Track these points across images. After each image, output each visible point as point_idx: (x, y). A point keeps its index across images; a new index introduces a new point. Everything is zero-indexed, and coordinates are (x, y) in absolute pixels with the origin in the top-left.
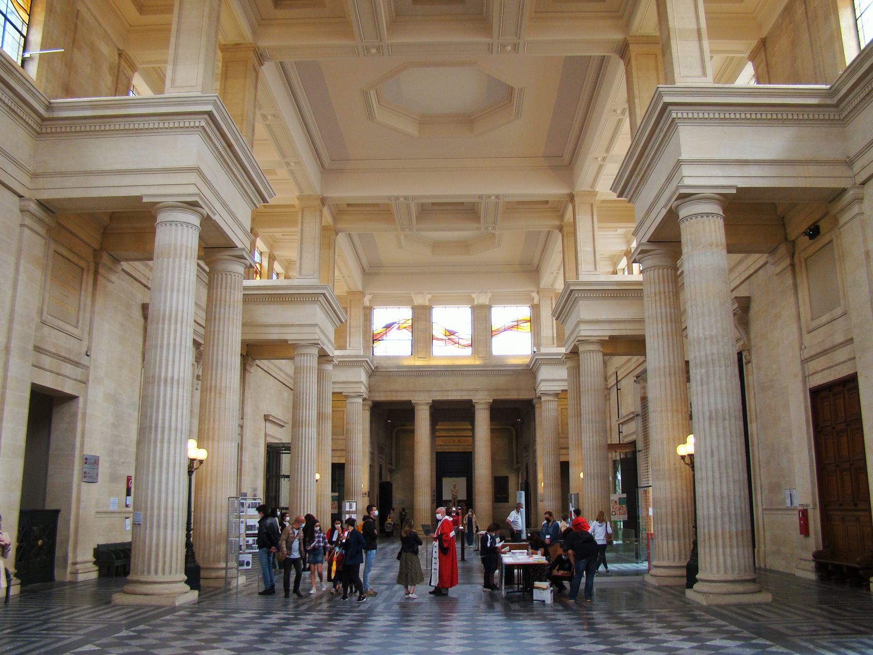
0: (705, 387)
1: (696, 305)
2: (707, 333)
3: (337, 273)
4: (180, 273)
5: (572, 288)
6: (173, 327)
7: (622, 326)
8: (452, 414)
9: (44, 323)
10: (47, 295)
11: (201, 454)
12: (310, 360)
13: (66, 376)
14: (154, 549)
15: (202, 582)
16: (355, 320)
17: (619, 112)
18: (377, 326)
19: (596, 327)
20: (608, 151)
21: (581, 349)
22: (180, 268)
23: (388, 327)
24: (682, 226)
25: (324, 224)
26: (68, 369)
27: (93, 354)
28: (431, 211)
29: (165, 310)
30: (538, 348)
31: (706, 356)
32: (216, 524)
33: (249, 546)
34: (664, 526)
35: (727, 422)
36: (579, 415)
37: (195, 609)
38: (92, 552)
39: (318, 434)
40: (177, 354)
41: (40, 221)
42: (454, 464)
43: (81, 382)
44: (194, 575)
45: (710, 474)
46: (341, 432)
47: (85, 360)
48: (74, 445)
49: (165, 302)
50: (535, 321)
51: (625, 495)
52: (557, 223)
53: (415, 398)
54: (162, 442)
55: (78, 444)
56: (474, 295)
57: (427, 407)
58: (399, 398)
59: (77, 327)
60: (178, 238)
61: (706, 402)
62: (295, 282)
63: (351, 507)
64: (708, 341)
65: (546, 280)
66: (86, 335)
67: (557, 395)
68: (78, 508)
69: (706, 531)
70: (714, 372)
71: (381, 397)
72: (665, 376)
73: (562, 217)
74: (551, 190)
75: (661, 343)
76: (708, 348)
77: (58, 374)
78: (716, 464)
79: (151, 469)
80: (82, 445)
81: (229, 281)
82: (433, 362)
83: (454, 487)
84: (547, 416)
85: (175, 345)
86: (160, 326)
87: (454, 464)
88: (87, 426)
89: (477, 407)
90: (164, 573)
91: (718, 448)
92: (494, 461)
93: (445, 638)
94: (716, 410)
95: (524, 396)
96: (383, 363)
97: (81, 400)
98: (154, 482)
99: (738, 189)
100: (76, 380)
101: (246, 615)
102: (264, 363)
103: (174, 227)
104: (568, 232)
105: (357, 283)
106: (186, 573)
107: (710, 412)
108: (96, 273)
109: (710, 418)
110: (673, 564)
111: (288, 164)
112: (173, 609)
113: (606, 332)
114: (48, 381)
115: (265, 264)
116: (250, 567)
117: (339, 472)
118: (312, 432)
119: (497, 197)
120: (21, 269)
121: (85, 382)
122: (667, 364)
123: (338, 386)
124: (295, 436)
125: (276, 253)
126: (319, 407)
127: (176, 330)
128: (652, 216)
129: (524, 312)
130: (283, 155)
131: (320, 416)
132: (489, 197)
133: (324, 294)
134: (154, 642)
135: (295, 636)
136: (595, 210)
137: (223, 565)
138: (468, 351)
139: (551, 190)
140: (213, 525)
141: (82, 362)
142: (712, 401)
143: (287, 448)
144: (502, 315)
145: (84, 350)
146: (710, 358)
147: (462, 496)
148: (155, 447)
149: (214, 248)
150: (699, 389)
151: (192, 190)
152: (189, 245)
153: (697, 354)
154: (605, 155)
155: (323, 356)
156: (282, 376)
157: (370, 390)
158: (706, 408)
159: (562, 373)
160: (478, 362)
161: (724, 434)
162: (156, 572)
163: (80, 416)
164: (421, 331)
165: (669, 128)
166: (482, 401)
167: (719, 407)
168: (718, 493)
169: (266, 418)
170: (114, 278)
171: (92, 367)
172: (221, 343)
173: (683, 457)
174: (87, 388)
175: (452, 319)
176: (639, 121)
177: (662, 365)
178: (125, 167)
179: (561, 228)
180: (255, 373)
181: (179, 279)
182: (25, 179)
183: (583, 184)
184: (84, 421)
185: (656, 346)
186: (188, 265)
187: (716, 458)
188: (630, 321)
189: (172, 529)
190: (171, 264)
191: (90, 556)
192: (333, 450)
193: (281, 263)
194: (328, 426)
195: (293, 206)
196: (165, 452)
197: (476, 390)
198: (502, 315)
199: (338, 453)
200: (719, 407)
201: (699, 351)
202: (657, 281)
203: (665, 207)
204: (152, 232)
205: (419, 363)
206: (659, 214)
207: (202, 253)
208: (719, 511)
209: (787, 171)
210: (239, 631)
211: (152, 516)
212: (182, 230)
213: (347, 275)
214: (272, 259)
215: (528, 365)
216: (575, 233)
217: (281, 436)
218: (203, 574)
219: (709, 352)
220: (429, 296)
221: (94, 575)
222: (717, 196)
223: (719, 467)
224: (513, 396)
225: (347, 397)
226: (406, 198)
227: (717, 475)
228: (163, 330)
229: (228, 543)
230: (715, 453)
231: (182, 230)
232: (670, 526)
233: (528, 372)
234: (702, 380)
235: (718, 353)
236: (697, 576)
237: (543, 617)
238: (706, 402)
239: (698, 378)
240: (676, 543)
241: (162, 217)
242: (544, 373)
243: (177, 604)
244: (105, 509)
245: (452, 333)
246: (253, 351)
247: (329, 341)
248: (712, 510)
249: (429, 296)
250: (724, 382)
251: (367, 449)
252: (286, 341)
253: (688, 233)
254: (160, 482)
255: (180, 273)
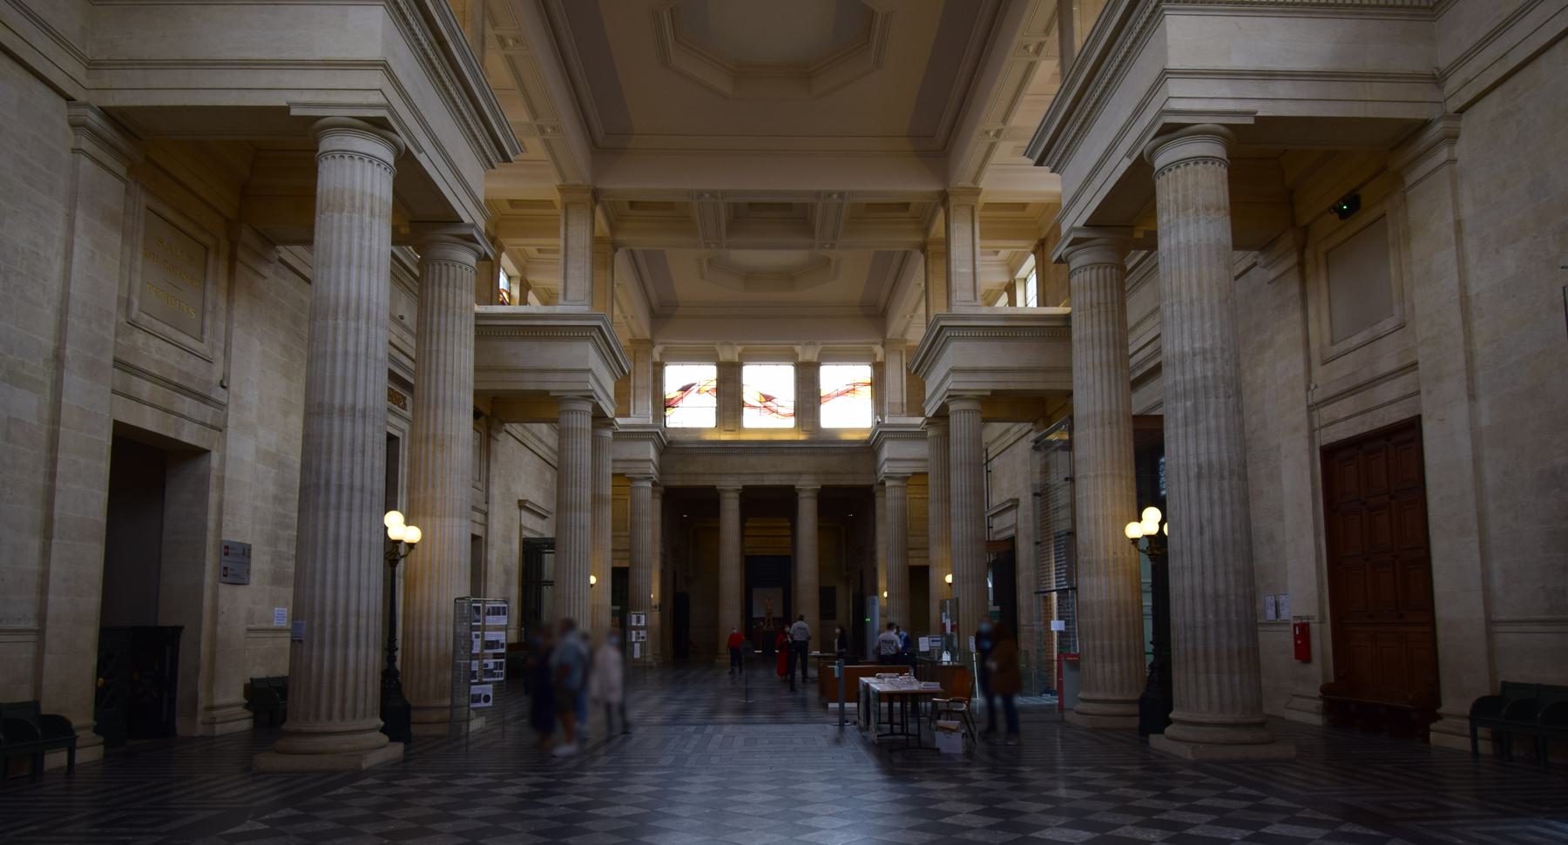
0: (1190, 429)
1: (1180, 303)
2: (1197, 345)
3: (616, 311)
4: (362, 237)
5: (942, 323)
6: (352, 325)
7: (1009, 377)
8: (772, 504)
9: (133, 324)
10: (138, 281)
11: (412, 534)
12: (582, 421)
13: (183, 416)
14: (326, 679)
15: (414, 729)
16: (643, 379)
17: (1031, 49)
18: (671, 389)
19: (973, 378)
20: (1005, 120)
21: (952, 408)
22: (362, 230)
23: (685, 389)
24: (1160, 182)
25: (598, 234)
26: (187, 405)
27: (234, 385)
28: (750, 216)
29: (337, 298)
30: (883, 418)
31: (1195, 380)
32: (437, 641)
33: (489, 673)
34: (1098, 643)
35: (1226, 483)
36: (946, 499)
37: (390, 773)
38: (241, 690)
39: (594, 524)
40: (362, 369)
41: (113, 149)
42: (771, 571)
43: (212, 427)
44: (397, 715)
45: (1197, 561)
46: (625, 528)
47: (218, 394)
48: (205, 527)
49: (338, 284)
50: (878, 384)
51: (997, 608)
52: (919, 239)
53: (723, 483)
54: (338, 508)
55: (211, 524)
56: (798, 349)
57: (736, 495)
58: (700, 483)
59: (202, 341)
60: (358, 183)
61: (1192, 451)
62: (558, 309)
63: (638, 620)
64: (1199, 358)
65: (895, 327)
66: (219, 355)
67: (905, 478)
68: (215, 622)
69: (1190, 645)
70: (1207, 405)
71: (677, 481)
72: (1103, 425)
73: (926, 230)
74: (914, 185)
75: (1098, 377)
76: (1198, 369)
77: (167, 411)
78: (1207, 547)
79: (319, 553)
80: (219, 525)
81: (452, 275)
82: (744, 437)
83: (767, 604)
84: (889, 506)
85: (356, 355)
86: (331, 322)
87: (771, 571)
88: (226, 496)
89: (801, 495)
90: (343, 717)
91: (1211, 521)
92: (822, 570)
93: (811, 816)
94: (1210, 463)
95: (862, 481)
96: (678, 437)
97: (215, 458)
98: (324, 573)
99: (1258, 119)
100: (203, 424)
101: (477, 781)
102: (516, 428)
103: (347, 160)
104: (937, 253)
105: (643, 328)
106: (382, 718)
107: (1200, 467)
108: (232, 259)
109: (1199, 476)
110: (1112, 697)
111: (542, 130)
112: (359, 774)
113: (986, 384)
114: (149, 421)
115: (516, 292)
116: (490, 704)
117: (621, 579)
118: (586, 518)
119: (841, 195)
120: (79, 224)
121: (220, 429)
122: (1107, 408)
123: (620, 465)
124: (559, 526)
125: (531, 279)
126: (594, 487)
127: (357, 330)
128: (1097, 182)
129: (864, 372)
130: (534, 113)
131: (597, 499)
132: (830, 195)
133: (599, 327)
134: (331, 826)
135: (554, 818)
136: (977, 214)
137: (447, 702)
138: (790, 423)
139: (914, 185)
140: (433, 643)
141: (213, 396)
142: (1203, 449)
143: (550, 544)
144: (832, 376)
145: (217, 377)
146: (1200, 384)
147: (778, 613)
148: (326, 516)
149: (421, 217)
150: (1181, 431)
151: (376, 98)
152: (377, 193)
153: (1179, 377)
154: (1000, 126)
155: (599, 418)
156: (543, 450)
157: (661, 470)
158: (1192, 460)
159: (919, 450)
160: (802, 437)
161: (1221, 499)
162: (330, 717)
163: (213, 480)
164: (729, 398)
165: (1146, 22)
166: (807, 485)
167: (1214, 458)
168: (1209, 589)
169: (522, 505)
170: (266, 271)
171: (231, 406)
172: (441, 369)
173: (1135, 541)
174: (225, 437)
175: (769, 386)
176: (1078, 43)
177: (1098, 408)
178: (255, 55)
179: (923, 248)
180: (506, 446)
181: (361, 247)
182: (79, 72)
183: (962, 180)
184: (221, 487)
185: (1090, 381)
186: (376, 228)
187: (1207, 537)
188: (1020, 371)
189: (358, 647)
190: (345, 222)
191: (237, 696)
192: (614, 551)
193: (537, 295)
194: (607, 513)
195: (549, 204)
196: (344, 523)
197: (800, 473)
198: (832, 376)
199: (621, 555)
200: (1214, 458)
201: (1183, 374)
202: (1094, 285)
203: (1129, 155)
204: (312, 172)
205: (726, 437)
206: (1120, 165)
207: (405, 230)
208: (1211, 616)
209: (1336, 89)
210: (459, 813)
211: (322, 626)
212: (363, 168)
213: (627, 317)
214: (525, 287)
215: (867, 442)
216: (946, 254)
217: (540, 528)
218: (415, 716)
219: (1199, 375)
220: (739, 349)
221: (245, 725)
222: (1223, 129)
223: (1213, 550)
224: (847, 481)
225: (631, 480)
226: (713, 194)
227: (1209, 562)
228: (335, 329)
229: (455, 667)
230: (1206, 529)
231: (363, 168)
232: (1106, 642)
233: (866, 450)
234: (1186, 417)
235: (1214, 376)
236: (1171, 715)
237: (951, 776)
238: (1192, 451)
239: (1180, 415)
240: (1116, 667)
241: (329, 143)
242: (888, 450)
243: (364, 766)
244: (265, 625)
245: (768, 398)
246: (496, 411)
247: (608, 396)
248: (1199, 615)
249: (739, 349)
250: (1223, 420)
251: (658, 549)
252: (547, 392)
253: (1168, 192)
254: (336, 574)
255: (362, 237)
